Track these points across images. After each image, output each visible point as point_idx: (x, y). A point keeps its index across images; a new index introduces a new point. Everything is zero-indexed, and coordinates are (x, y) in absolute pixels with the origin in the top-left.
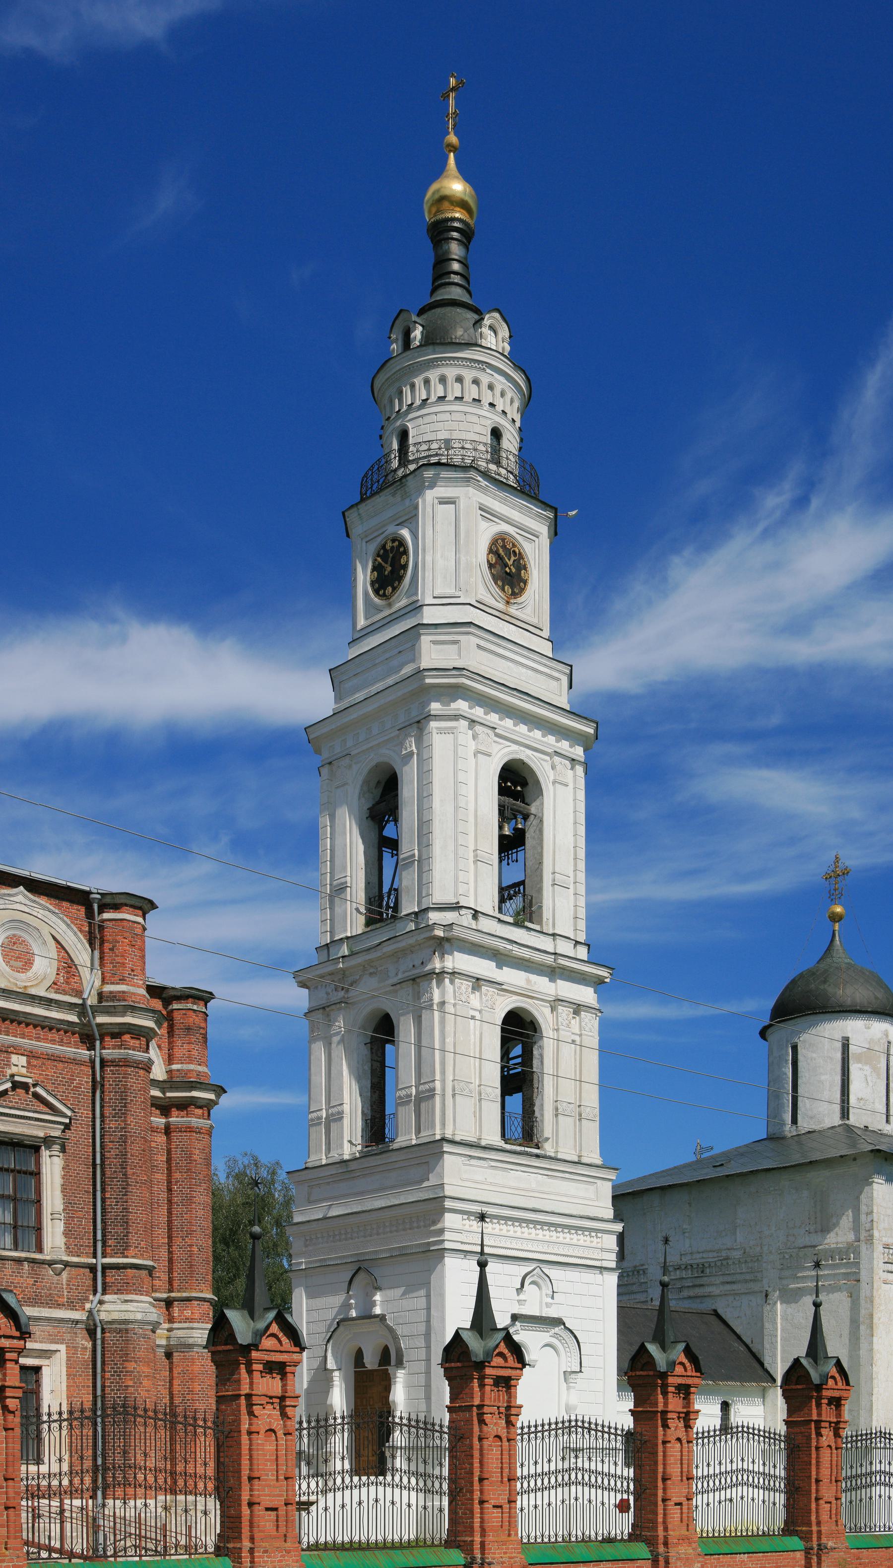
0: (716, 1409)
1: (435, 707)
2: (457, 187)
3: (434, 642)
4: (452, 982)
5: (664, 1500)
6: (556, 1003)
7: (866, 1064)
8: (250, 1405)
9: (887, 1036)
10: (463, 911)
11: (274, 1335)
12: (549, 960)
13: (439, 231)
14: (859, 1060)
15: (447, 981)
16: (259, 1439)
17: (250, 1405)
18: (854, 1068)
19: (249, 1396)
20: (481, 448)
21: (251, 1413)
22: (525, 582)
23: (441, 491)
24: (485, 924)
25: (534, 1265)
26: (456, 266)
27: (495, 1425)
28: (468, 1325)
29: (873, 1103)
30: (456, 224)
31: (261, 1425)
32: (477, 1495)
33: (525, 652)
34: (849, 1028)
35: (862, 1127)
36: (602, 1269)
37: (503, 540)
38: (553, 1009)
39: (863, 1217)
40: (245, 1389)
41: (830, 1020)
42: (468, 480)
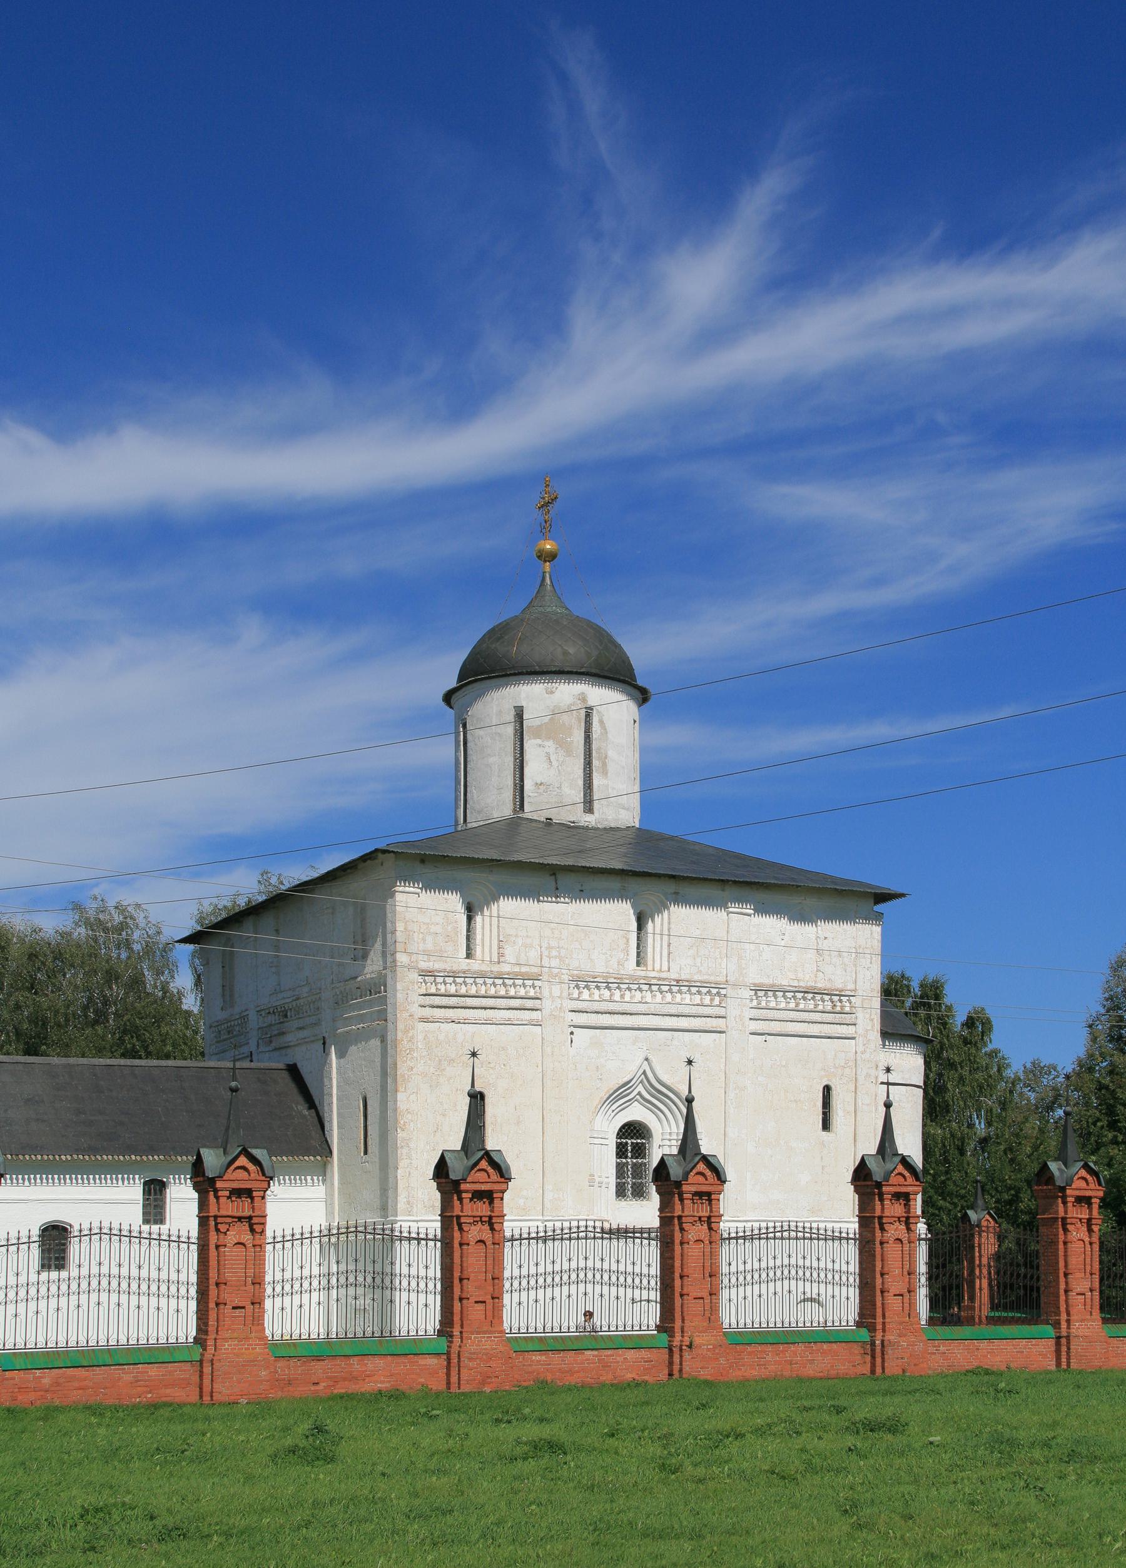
4: (341, 1055)
5: (1066, 1291)
7: (548, 738)
8: (681, 1224)
11: (900, 1174)
16: (470, 1249)
17: (681, 1224)
18: (531, 745)
19: (880, 1218)
21: (682, 1229)
27: (696, 1231)
28: (873, 1151)
29: (560, 788)
31: (691, 1236)
32: (1062, 1286)
34: (523, 695)
35: (543, 819)
39: (389, 936)
40: (878, 1213)
41: (498, 687)
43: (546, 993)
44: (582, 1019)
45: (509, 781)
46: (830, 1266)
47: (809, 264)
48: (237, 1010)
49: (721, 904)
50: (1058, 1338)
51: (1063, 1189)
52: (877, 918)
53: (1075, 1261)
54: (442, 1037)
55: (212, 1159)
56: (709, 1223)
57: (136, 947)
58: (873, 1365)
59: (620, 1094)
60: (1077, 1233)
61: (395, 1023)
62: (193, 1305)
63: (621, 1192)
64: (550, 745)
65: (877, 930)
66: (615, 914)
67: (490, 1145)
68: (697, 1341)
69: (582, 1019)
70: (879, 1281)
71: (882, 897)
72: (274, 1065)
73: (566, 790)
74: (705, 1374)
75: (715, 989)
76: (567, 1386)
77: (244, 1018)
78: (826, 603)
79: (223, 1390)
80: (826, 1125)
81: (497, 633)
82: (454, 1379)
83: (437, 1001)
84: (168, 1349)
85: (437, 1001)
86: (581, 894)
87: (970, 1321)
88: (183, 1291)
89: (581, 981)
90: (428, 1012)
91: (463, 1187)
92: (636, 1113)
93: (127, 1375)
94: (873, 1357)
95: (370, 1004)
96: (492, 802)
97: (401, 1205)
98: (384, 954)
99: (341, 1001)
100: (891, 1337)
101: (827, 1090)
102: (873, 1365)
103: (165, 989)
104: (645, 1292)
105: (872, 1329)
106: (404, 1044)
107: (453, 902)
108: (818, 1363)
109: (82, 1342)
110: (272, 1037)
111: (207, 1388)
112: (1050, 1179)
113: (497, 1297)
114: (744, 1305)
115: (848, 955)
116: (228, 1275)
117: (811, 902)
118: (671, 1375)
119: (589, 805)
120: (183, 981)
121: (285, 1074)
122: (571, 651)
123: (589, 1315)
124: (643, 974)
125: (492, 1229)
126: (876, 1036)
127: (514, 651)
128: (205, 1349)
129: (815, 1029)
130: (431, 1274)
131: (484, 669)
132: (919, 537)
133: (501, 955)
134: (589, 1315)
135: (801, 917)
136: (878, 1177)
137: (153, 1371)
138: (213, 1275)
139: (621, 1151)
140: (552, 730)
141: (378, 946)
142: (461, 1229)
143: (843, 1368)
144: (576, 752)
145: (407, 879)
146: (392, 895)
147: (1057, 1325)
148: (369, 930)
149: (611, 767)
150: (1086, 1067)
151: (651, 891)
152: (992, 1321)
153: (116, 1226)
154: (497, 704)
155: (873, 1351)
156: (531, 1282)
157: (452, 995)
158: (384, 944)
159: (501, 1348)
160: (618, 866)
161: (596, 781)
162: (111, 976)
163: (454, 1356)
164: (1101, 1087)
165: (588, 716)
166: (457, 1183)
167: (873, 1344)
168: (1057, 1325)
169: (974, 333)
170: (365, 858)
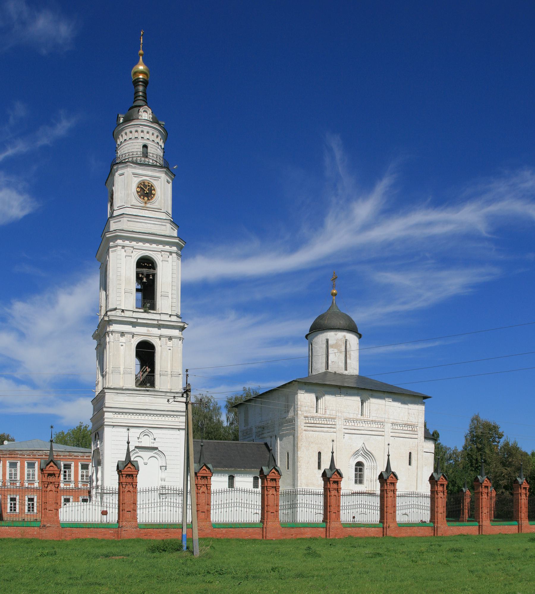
0: (226, 479)
1: (111, 244)
2: (141, 68)
3: (114, 222)
4: (281, 440)
6: (160, 337)
9: (345, 337)
10: (117, 310)
12: (156, 322)
13: (136, 83)
14: (332, 347)
15: (110, 334)
18: (330, 350)
20: (139, 153)
21: (387, 493)
22: (154, 195)
23: (120, 172)
24: (127, 314)
25: (145, 429)
26: (141, 94)
30: (141, 80)
31: (389, 495)
33: (149, 219)
36: (179, 429)
37: (144, 182)
38: (160, 339)
41: (321, 333)
42: (127, 166)
43: (337, 423)
44: (347, 431)
45: (324, 360)
46: (240, 501)
47: (393, 208)
48: (249, 427)
49: (383, 398)
50: (479, 526)
51: (481, 484)
52: (423, 403)
53: (484, 504)
54: (310, 435)
55: (265, 470)
56: (394, 491)
57: (211, 408)
58: (434, 533)
59: (356, 453)
60: (523, 497)
61: (297, 431)
62: (181, 510)
63: (356, 482)
64: (336, 351)
65: (424, 407)
66: (354, 401)
67: (337, 467)
68: (391, 525)
69: (347, 431)
70: (385, 509)
71: (425, 398)
72: (261, 443)
73: (340, 364)
74: (392, 535)
75: (382, 423)
76: (354, 537)
77: (251, 429)
78: (390, 309)
79: (269, 536)
80: (410, 464)
81: (321, 317)
82: (328, 535)
83: (309, 425)
84: (254, 524)
85: (309, 425)
86: (347, 394)
87: (463, 521)
88: (114, 506)
89: (347, 420)
90: (306, 428)
91: (331, 479)
92: (360, 459)
93: (244, 530)
94: (434, 531)
95: (290, 425)
96: (319, 367)
97: (299, 484)
98: (294, 411)
99: (281, 425)
100: (439, 525)
101: (410, 453)
102: (434, 533)
103: (219, 420)
104: (255, 510)
105: (383, 523)
106: (300, 438)
107: (313, 396)
108: (420, 532)
109: (243, 521)
110: (260, 435)
111: (264, 535)
112: (478, 481)
113: (339, 512)
114: (402, 516)
115: (415, 414)
116: (270, 503)
117: (407, 398)
118: (383, 535)
119: (346, 369)
120: (223, 418)
121: (264, 446)
122: (342, 322)
123: (354, 517)
124: (362, 418)
125: (338, 492)
126: (423, 438)
127: (326, 322)
128: (264, 524)
129: (407, 436)
130: (258, 504)
131: (317, 328)
132: (418, 289)
133: (325, 412)
134: (354, 517)
135: (404, 403)
136: (436, 479)
137: (251, 530)
138: (266, 503)
139: (356, 470)
140: (336, 346)
141: (292, 408)
142: (330, 491)
143: (426, 534)
144: (341, 353)
145: (301, 389)
146: (297, 394)
147: (479, 522)
148: (290, 403)
149: (352, 357)
150: (465, 448)
151: (365, 394)
152: (468, 521)
153: (246, 489)
154: (321, 339)
155: (326, 529)
156: (348, 507)
157: (314, 424)
158: (294, 408)
159: (340, 526)
160: (355, 386)
161: (348, 361)
162: (205, 417)
163: (328, 528)
164: (468, 454)
165: (346, 342)
166: (329, 478)
167: (434, 527)
168: (479, 522)
169: (437, 230)
170: (289, 383)
